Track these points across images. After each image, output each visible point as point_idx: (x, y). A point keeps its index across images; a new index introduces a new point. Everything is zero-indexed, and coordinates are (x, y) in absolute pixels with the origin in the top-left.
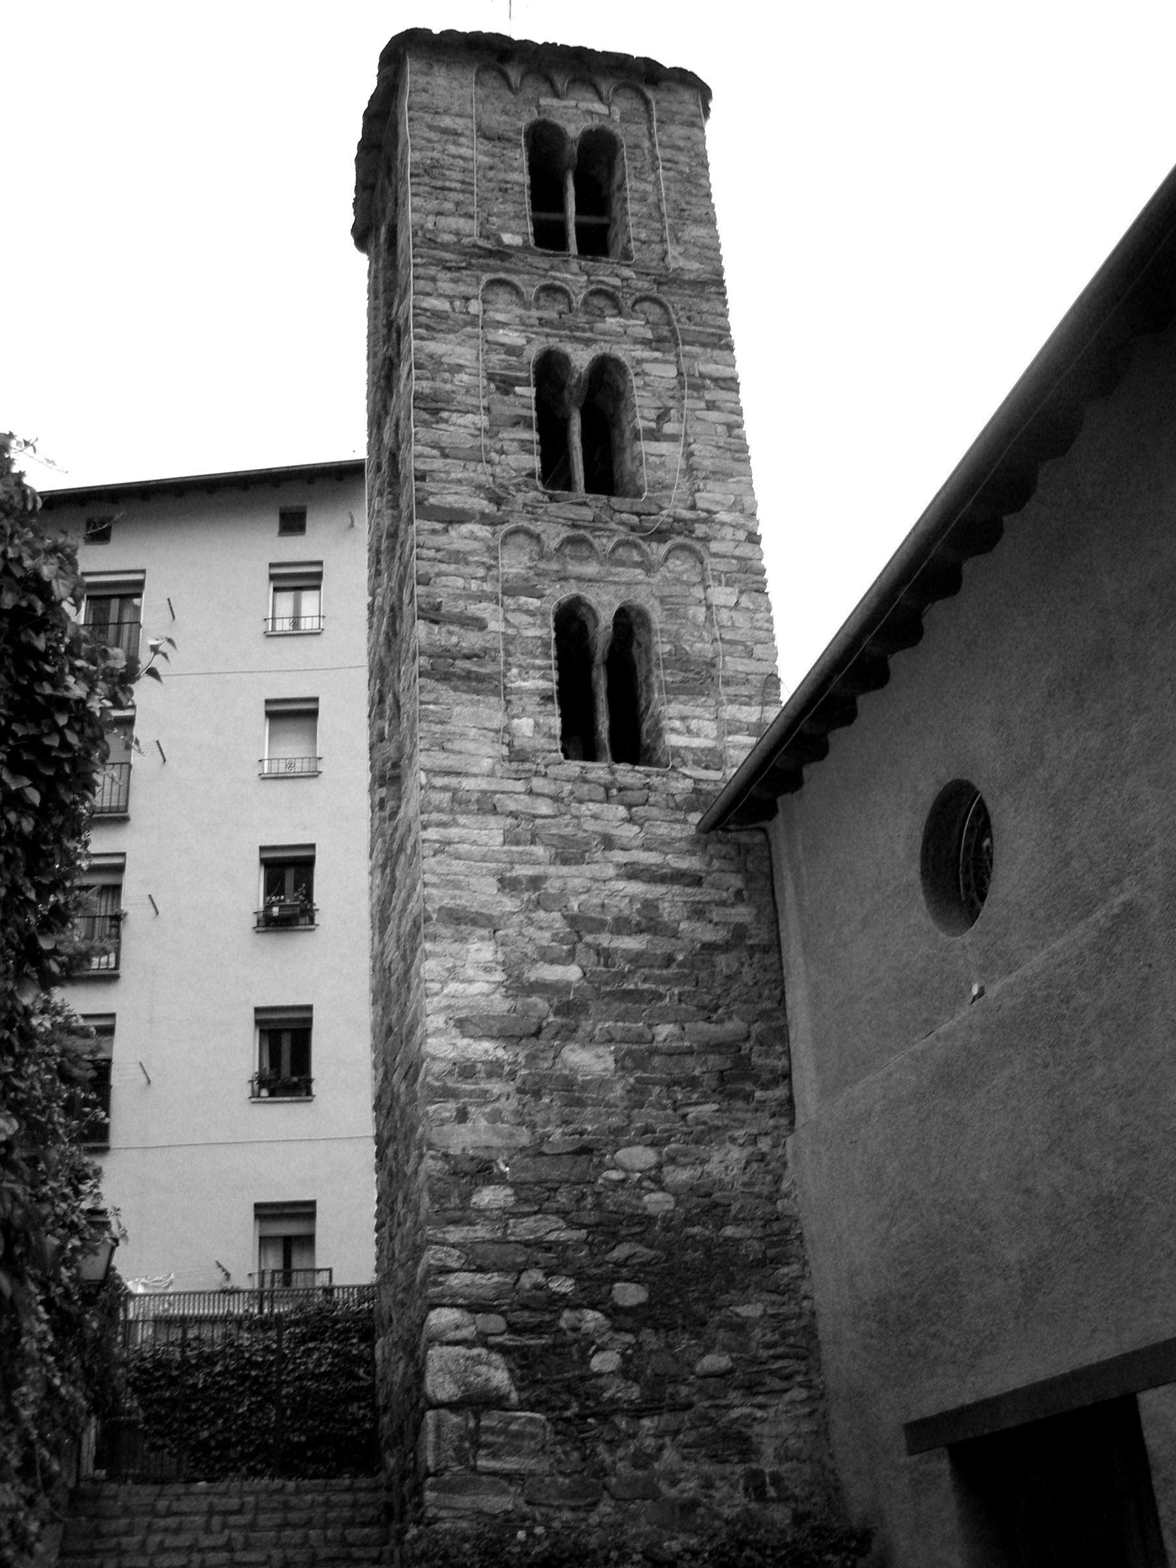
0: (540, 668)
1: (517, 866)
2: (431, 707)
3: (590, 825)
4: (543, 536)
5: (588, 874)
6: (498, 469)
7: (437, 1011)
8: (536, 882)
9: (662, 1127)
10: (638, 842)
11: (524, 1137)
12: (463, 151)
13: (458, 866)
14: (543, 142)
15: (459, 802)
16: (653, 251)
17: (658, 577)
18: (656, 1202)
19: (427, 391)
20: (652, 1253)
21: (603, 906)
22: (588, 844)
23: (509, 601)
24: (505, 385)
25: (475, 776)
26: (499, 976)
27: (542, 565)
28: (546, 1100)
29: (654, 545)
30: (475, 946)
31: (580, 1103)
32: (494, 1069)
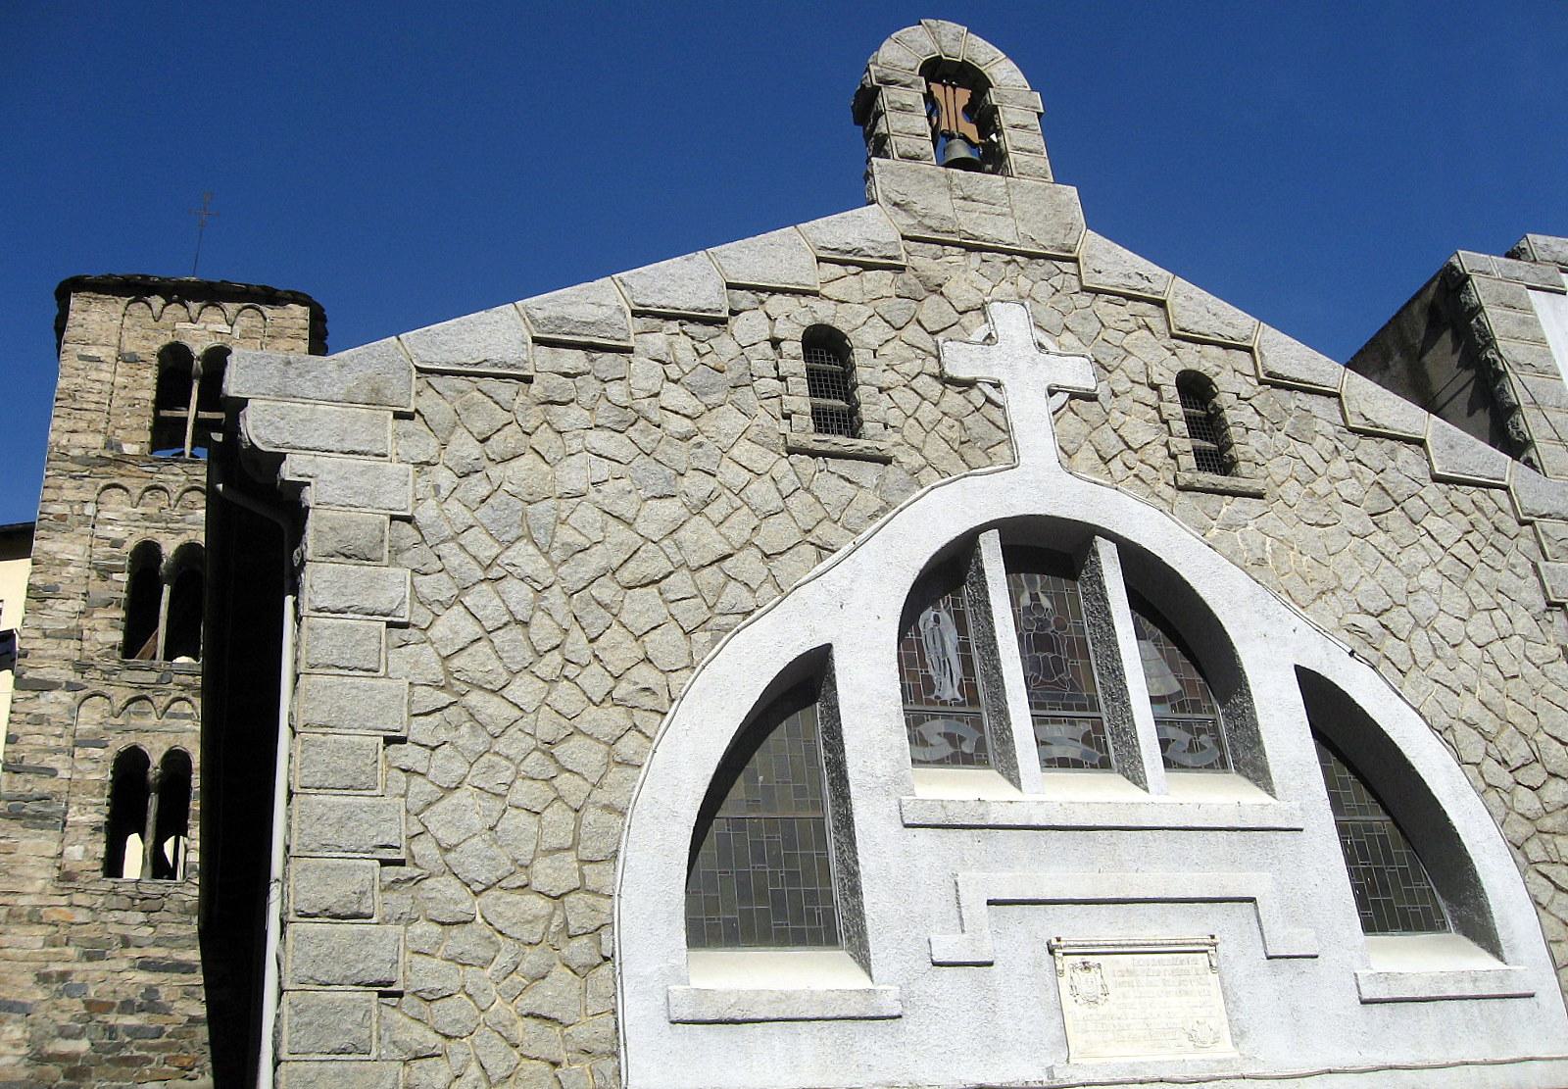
1: (51, 964)
3: (114, 929)
8: (64, 976)
21: (115, 992)
22: (110, 944)
23: (78, 752)
25: (29, 894)
26: (23, 1051)
27: (112, 721)
30: (8, 1029)
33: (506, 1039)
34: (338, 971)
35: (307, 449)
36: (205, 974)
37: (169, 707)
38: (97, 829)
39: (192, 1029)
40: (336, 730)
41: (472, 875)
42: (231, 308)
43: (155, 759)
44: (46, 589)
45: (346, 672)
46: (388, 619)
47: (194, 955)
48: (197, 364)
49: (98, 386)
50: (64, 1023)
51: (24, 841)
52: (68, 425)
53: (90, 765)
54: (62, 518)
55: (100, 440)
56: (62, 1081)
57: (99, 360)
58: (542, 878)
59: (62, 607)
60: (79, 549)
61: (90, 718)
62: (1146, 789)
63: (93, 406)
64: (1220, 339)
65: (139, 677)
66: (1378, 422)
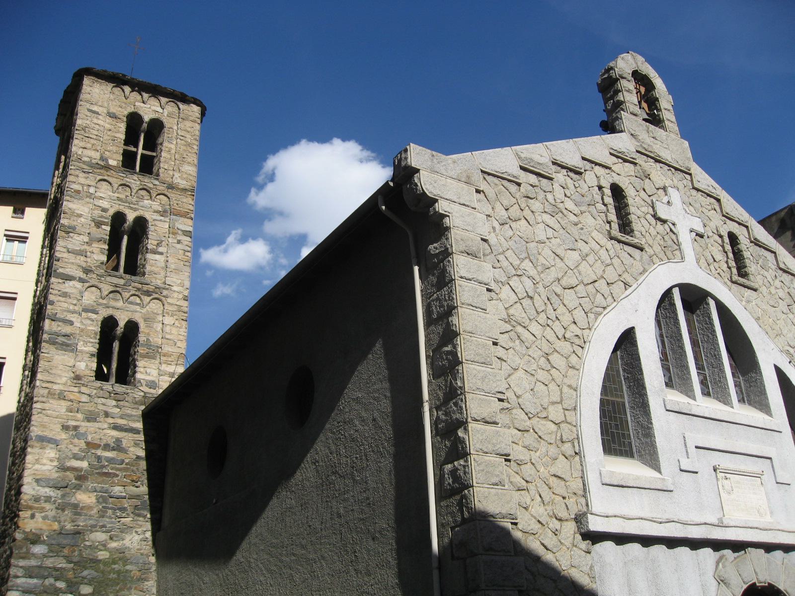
0: (92, 343)
1: (69, 421)
2: (46, 355)
3: (101, 407)
4: (103, 290)
5: (97, 426)
6: (89, 260)
7: (30, 475)
8: (76, 428)
9: (110, 525)
10: (119, 415)
11: (56, 526)
12: (100, 122)
13: (46, 419)
14: (134, 120)
15: (51, 394)
16: (169, 174)
17: (145, 310)
18: (103, 555)
19: (66, 224)
20: (98, 574)
21: (101, 439)
22: (99, 414)
23: (83, 314)
24: (98, 224)
25: (59, 384)
26: (56, 463)
27: (101, 301)
28: (66, 512)
29: (146, 297)
30: (48, 451)
31: (79, 514)
32: (48, 499)
33: (547, 485)
34: (490, 448)
35: (446, 199)
36: (145, 435)
37: (129, 298)
38: (93, 355)
39: (138, 462)
40: (475, 335)
41: (528, 410)
42: (164, 100)
43: (122, 324)
44: (69, 227)
45: (474, 309)
46: (487, 286)
47: (139, 425)
48: (145, 125)
49: (97, 127)
50: (75, 452)
51: (57, 356)
52: (82, 144)
53: (89, 322)
54: (78, 192)
55: (97, 155)
56: (74, 481)
57: (97, 113)
58: (552, 414)
59: (78, 238)
60: (87, 210)
61: (90, 297)
62: (732, 407)
63: (95, 137)
64: (738, 220)
65: (115, 280)
66: (789, 267)
